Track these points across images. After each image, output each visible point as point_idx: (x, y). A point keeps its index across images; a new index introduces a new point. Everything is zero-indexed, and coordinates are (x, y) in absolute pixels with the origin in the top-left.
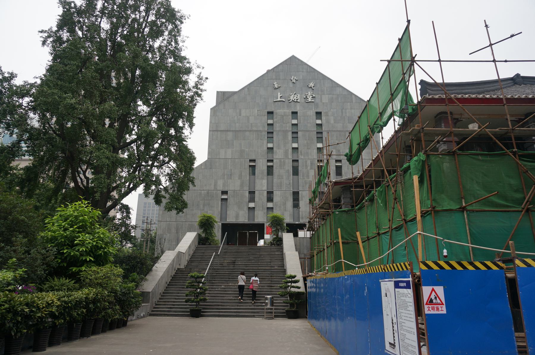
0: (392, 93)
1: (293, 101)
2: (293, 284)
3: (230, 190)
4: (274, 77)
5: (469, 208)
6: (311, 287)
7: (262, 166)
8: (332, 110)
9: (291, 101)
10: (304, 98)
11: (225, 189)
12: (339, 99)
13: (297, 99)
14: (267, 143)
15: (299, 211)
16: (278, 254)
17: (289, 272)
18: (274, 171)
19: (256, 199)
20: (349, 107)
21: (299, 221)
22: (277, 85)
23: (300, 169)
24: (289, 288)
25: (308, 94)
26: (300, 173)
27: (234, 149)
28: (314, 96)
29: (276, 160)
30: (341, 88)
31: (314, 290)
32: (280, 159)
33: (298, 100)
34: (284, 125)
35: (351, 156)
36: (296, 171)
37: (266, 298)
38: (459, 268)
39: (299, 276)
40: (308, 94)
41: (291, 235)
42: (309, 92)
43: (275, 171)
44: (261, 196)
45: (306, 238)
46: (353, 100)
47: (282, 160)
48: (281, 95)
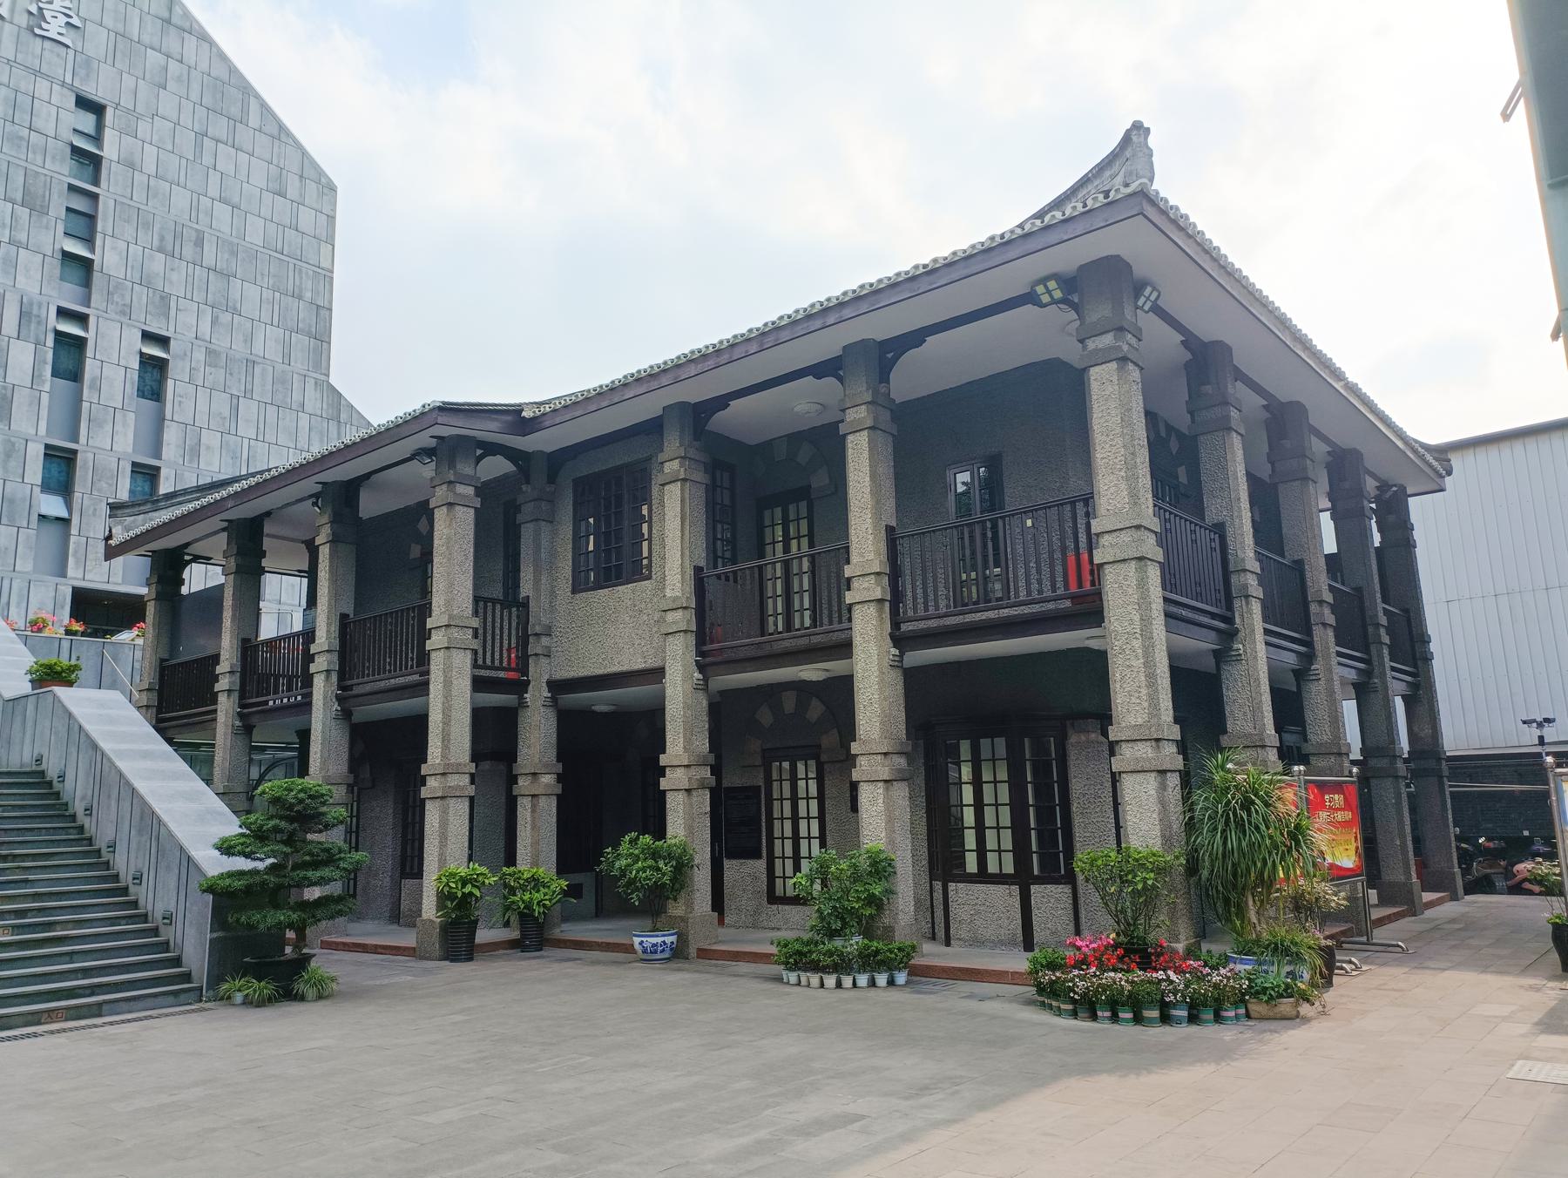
30: (206, 46)
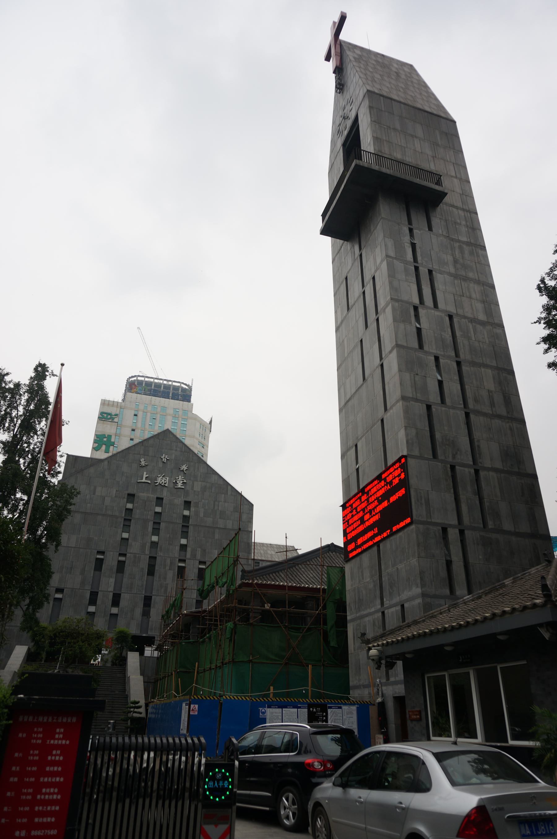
0: (229, 566)
1: (160, 484)
2: (136, 710)
3: (66, 588)
4: (142, 452)
5: (253, 661)
6: (152, 713)
7: (111, 560)
8: (203, 501)
9: (158, 484)
10: (174, 483)
11: (62, 586)
12: (213, 489)
13: (165, 482)
14: (123, 532)
15: (149, 621)
16: (121, 677)
17: (133, 698)
18: (125, 568)
19: (99, 602)
20: (223, 500)
21: (147, 633)
22: (144, 462)
23: (157, 568)
24: (132, 713)
25: (178, 479)
26: (157, 574)
27: (80, 536)
28: (185, 481)
29: (130, 555)
31: (153, 716)
32: (135, 553)
33: (166, 483)
34: (145, 512)
35: (203, 591)
36: (151, 572)
37: (110, 722)
38: (205, 699)
39: (142, 702)
40: (178, 479)
41: (137, 654)
42: (180, 477)
43: (128, 569)
44: (104, 599)
45: (153, 657)
46: (229, 491)
47: (137, 555)
48: (147, 476)
